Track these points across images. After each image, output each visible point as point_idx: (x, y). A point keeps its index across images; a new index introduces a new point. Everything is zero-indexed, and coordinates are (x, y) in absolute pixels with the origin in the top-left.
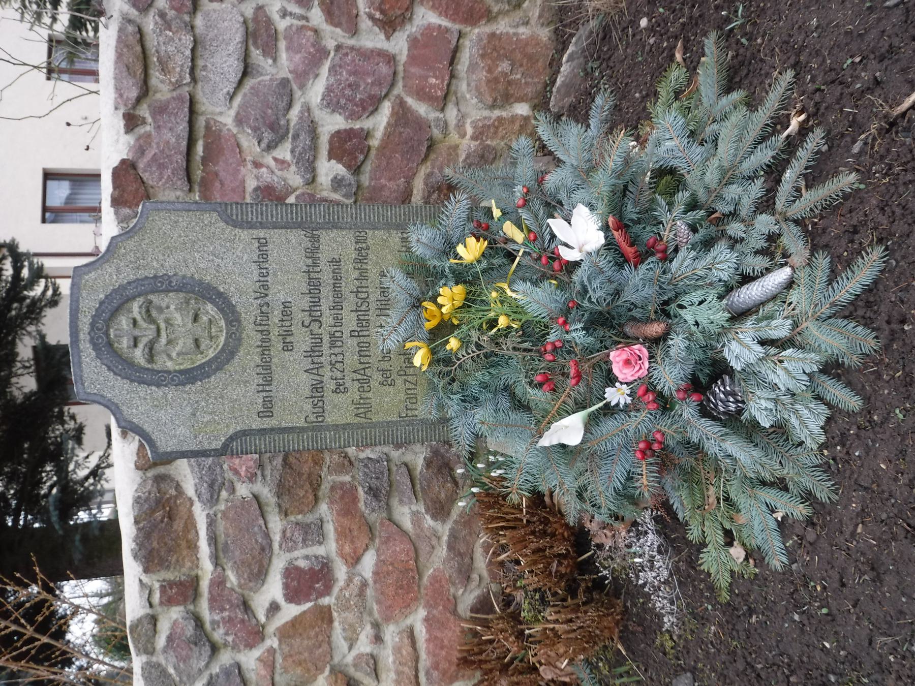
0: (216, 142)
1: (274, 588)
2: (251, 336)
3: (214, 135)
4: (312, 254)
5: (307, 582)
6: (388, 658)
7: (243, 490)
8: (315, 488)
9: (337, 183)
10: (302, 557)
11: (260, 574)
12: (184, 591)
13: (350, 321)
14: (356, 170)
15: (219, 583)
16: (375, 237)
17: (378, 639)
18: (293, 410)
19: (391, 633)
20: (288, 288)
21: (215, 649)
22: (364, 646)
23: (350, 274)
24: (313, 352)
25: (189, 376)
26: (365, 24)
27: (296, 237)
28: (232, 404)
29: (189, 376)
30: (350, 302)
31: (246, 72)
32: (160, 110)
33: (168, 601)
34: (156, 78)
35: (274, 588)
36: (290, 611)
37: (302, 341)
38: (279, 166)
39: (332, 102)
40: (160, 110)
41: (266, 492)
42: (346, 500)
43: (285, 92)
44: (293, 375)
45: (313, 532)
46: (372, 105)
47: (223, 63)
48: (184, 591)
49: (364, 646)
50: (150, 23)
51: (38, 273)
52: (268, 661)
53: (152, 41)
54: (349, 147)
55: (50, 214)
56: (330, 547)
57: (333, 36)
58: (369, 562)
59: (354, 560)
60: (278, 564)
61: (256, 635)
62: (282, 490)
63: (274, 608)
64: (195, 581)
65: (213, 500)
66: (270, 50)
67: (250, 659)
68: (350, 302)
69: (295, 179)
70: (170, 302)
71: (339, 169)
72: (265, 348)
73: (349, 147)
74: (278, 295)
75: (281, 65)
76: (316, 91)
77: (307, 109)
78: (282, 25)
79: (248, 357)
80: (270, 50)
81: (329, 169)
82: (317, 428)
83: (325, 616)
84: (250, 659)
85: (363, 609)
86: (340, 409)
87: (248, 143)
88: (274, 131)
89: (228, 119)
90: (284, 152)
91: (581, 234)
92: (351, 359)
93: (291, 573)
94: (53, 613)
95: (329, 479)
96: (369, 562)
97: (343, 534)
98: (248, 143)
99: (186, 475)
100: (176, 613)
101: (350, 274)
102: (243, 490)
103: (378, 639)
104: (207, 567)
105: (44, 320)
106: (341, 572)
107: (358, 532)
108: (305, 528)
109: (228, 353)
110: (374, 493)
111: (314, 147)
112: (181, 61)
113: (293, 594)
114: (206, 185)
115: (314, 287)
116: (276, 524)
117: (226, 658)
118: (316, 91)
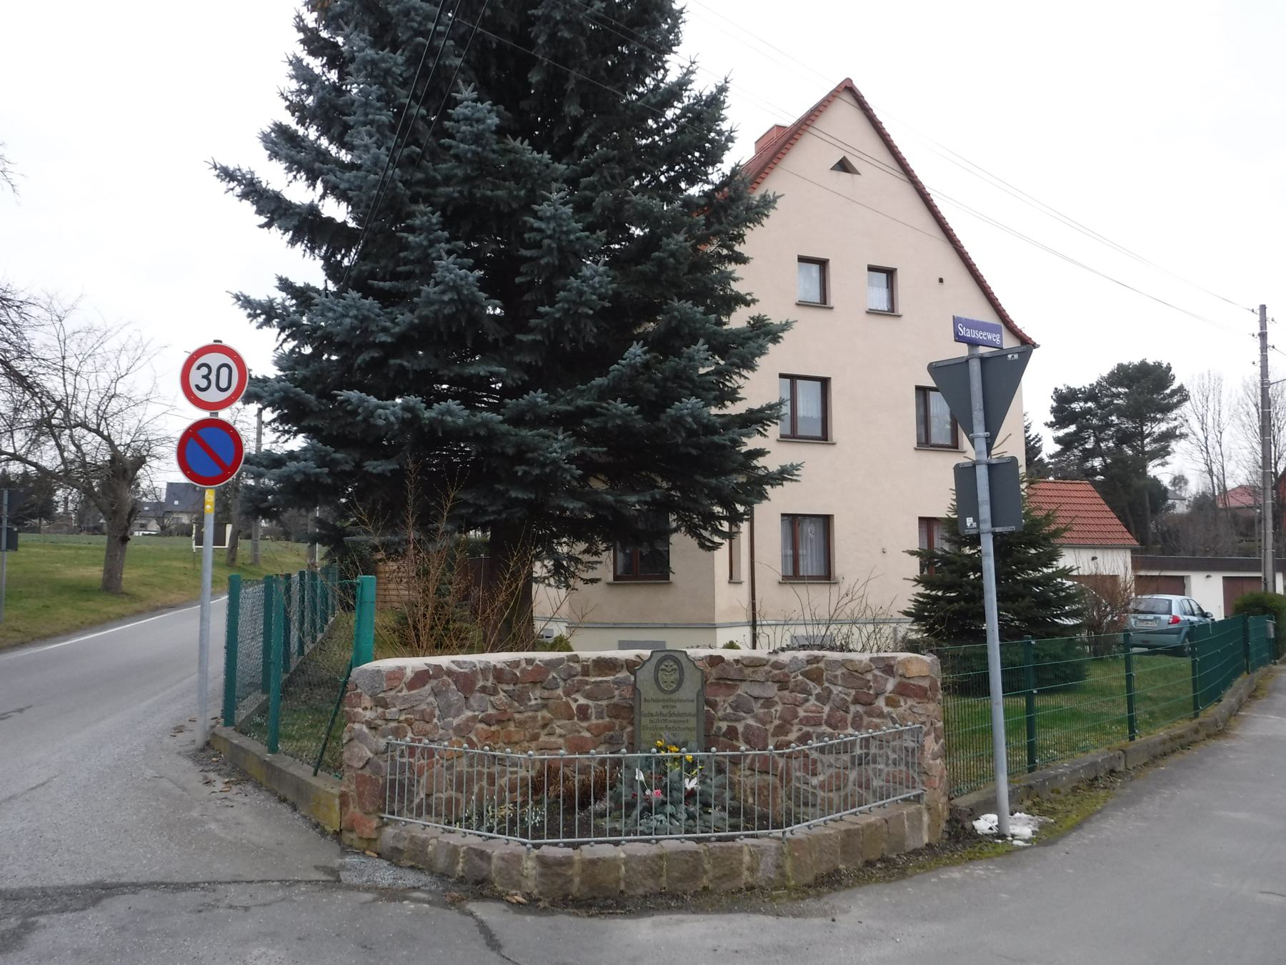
0: (732, 688)
1: (582, 701)
2: (666, 697)
3: (734, 687)
4: (690, 715)
5: (583, 712)
6: (553, 739)
7: (617, 692)
8: (616, 717)
9: (719, 728)
10: (592, 711)
11: (587, 697)
12: (586, 672)
13: (670, 725)
14: (724, 735)
15: (587, 683)
16: (694, 733)
17: (561, 736)
18: (645, 708)
19: (561, 741)
20: (680, 708)
21: (565, 680)
22: (558, 731)
23: (683, 726)
24: (661, 714)
25: (657, 680)
26: (776, 739)
27: (694, 711)
28: (648, 690)
29: (657, 680)
30: (676, 725)
31: (756, 698)
32: (741, 670)
33: (583, 667)
34: (751, 669)
35: (582, 701)
36: (574, 706)
37: (665, 711)
38: (724, 708)
39: (748, 727)
40: (741, 670)
41: (615, 700)
42: (610, 728)
43: (749, 711)
44: (655, 708)
45: (599, 716)
46: (747, 742)
47: (757, 691)
48: (586, 672)
49: (558, 731)
50: (767, 668)
51: (735, 519)
52: (559, 698)
53: (761, 669)
54: (732, 733)
55: (793, 521)
56: (594, 721)
57: (771, 728)
58: (587, 734)
59: (588, 730)
60: (590, 703)
61: (568, 694)
62: (616, 705)
63: (576, 700)
64: (588, 675)
65: (615, 683)
66: (763, 706)
67: (560, 692)
68: (676, 725)
69: (720, 714)
70: (677, 676)
71: (724, 729)
72: (664, 700)
73: (732, 733)
74: (678, 705)
75: (757, 708)
76: (751, 722)
77: (744, 719)
78: (773, 710)
79: (661, 696)
80: (763, 706)
81: (724, 725)
82: (640, 714)
83: (571, 718)
84: (560, 692)
85: (571, 732)
86: (645, 721)
87: (732, 698)
88: (736, 707)
89: (739, 692)
90: (729, 710)
91: (691, 784)
92: (659, 725)
93: (587, 707)
94: (291, 379)
95: (617, 722)
96: (587, 734)
97: (597, 726)
98: (732, 698)
99: (623, 674)
100: (579, 669)
101: (683, 726)
102: (617, 692)
103: (561, 736)
104: (593, 680)
105: (733, 314)
106: (585, 724)
107: (597, 732)
108: (602, 712)
109: (663, 691)
110: (612, 737)
111: (731, 721)
112: (756, 677)
113: (580, 707)
114: (718, 684)
115: (679, 715)
116: (604, 703)
117: (562, 684)
118: (751, 722)
